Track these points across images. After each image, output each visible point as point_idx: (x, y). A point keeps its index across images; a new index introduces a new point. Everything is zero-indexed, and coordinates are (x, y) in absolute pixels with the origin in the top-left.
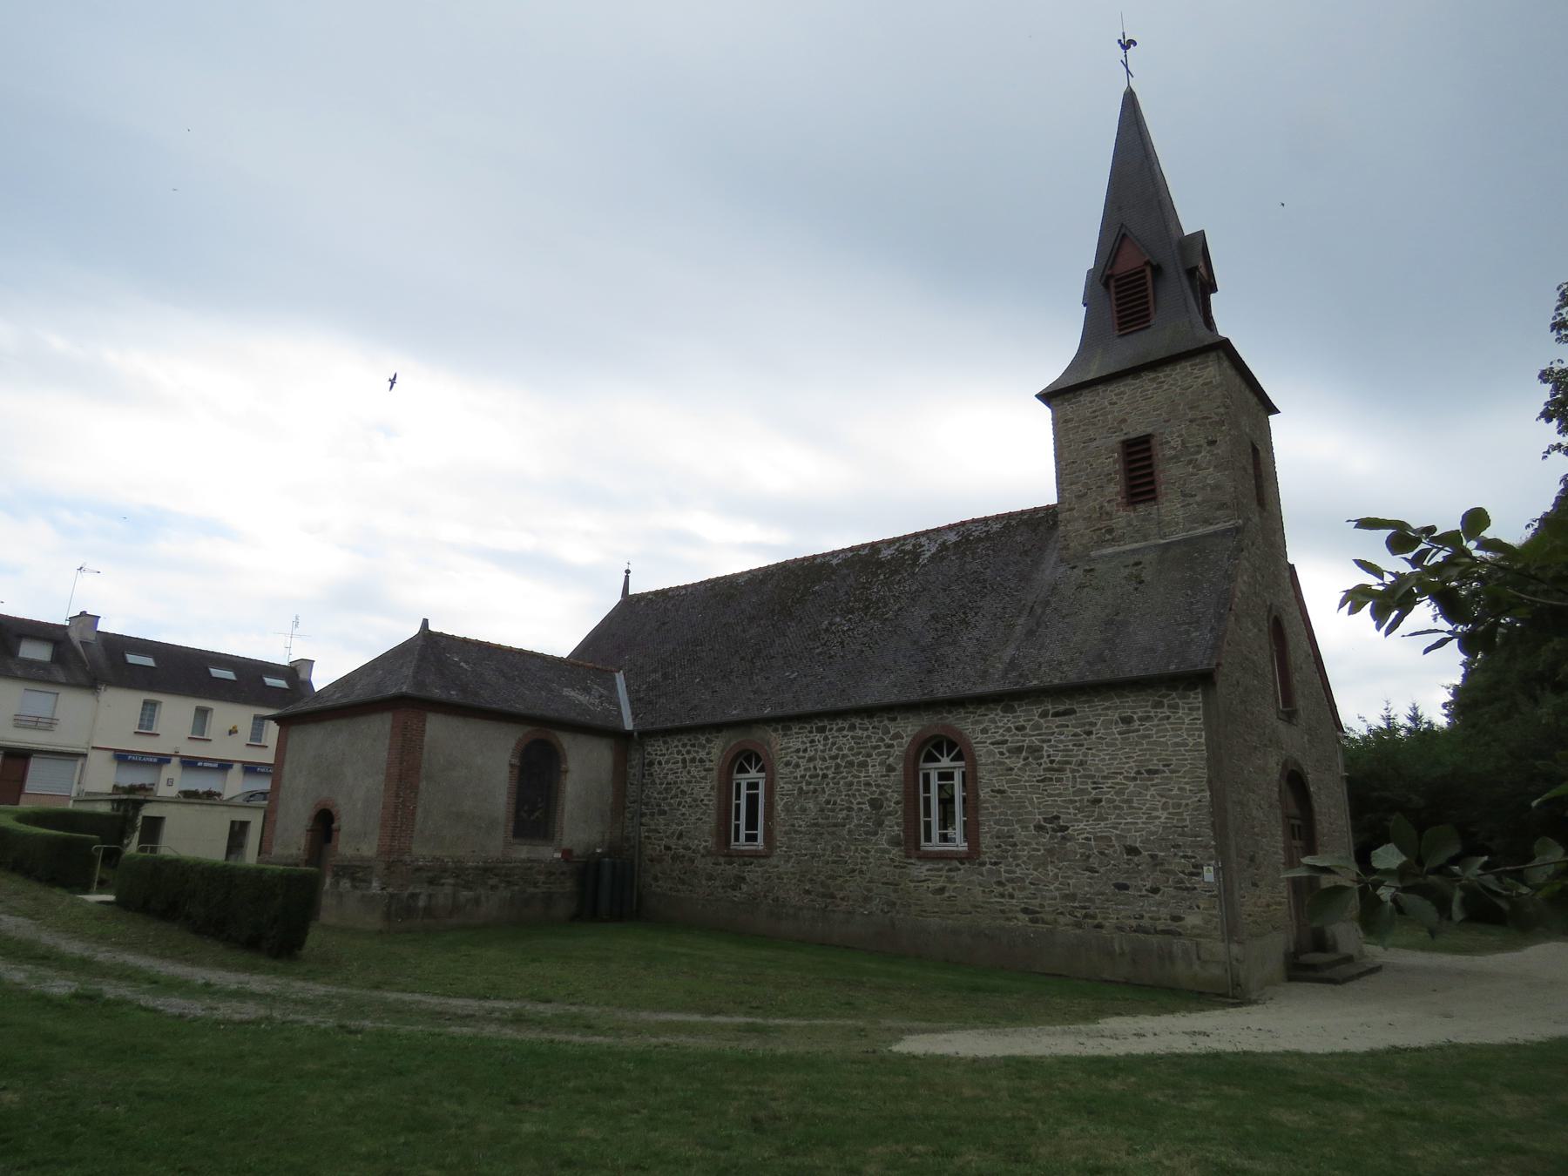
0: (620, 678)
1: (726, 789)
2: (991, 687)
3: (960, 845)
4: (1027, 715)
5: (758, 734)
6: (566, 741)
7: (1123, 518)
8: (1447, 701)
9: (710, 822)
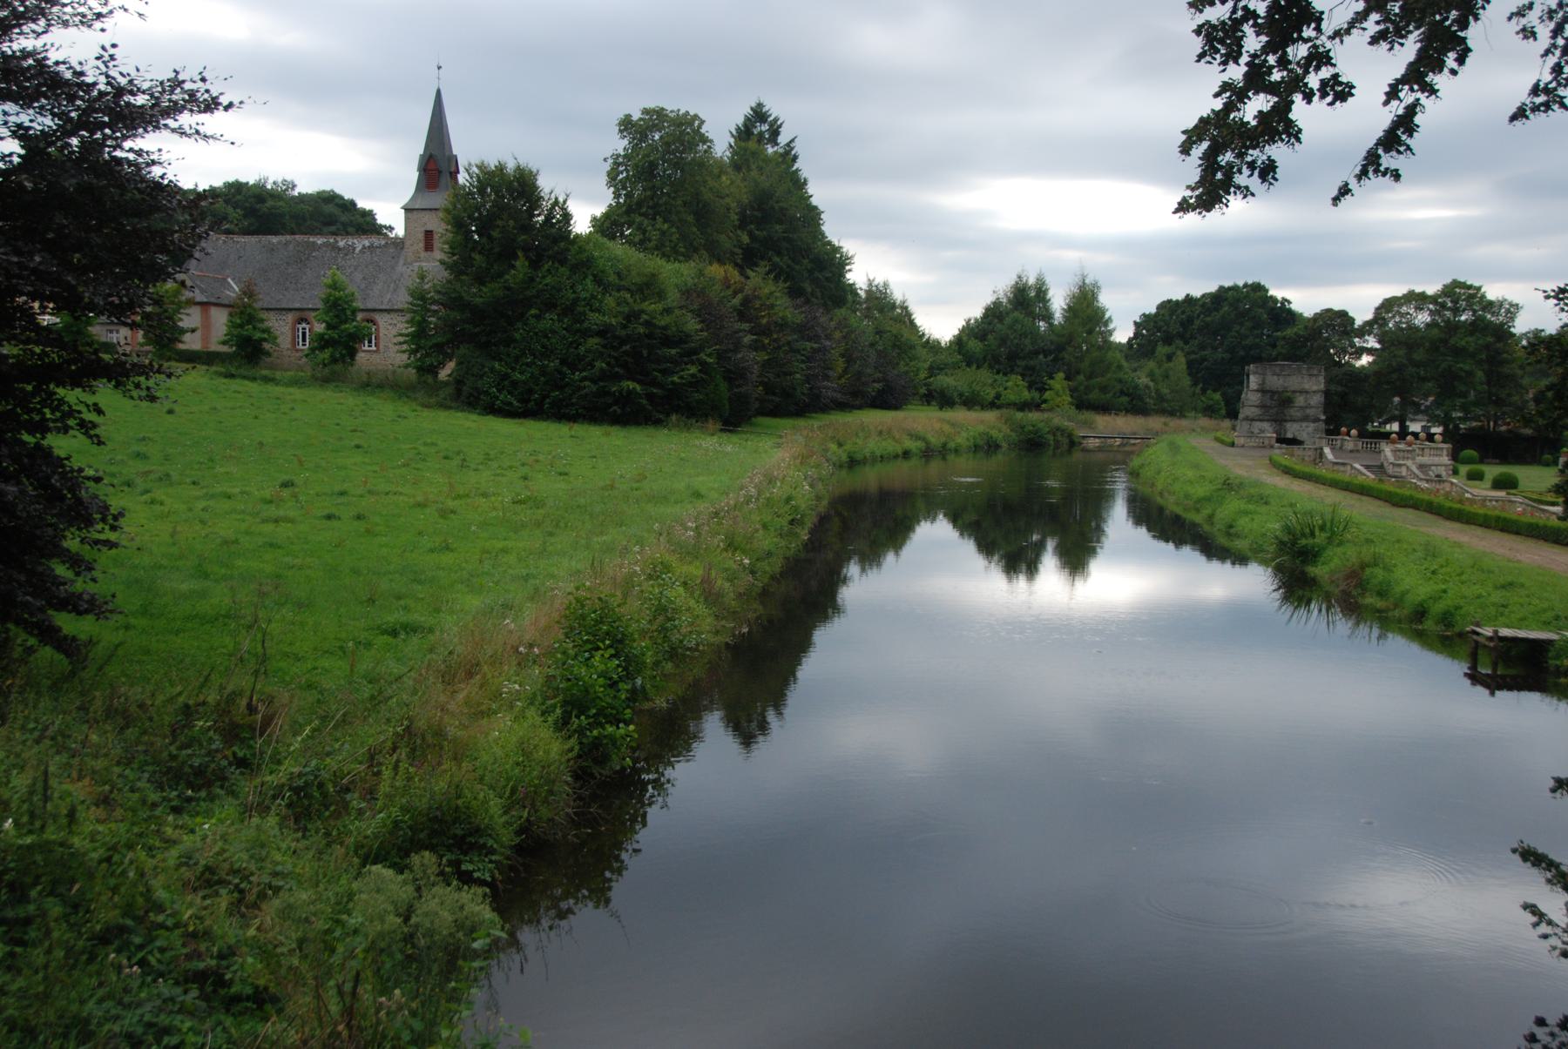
0: (229, 280)
1: (294, 330)
2: (384, 307)
3: (374, 348)
4: (393, 315)
5: (307, 313)
6: (378, 317)
7: (423, 254)
8: (703, 127)
9: (289, 339)
